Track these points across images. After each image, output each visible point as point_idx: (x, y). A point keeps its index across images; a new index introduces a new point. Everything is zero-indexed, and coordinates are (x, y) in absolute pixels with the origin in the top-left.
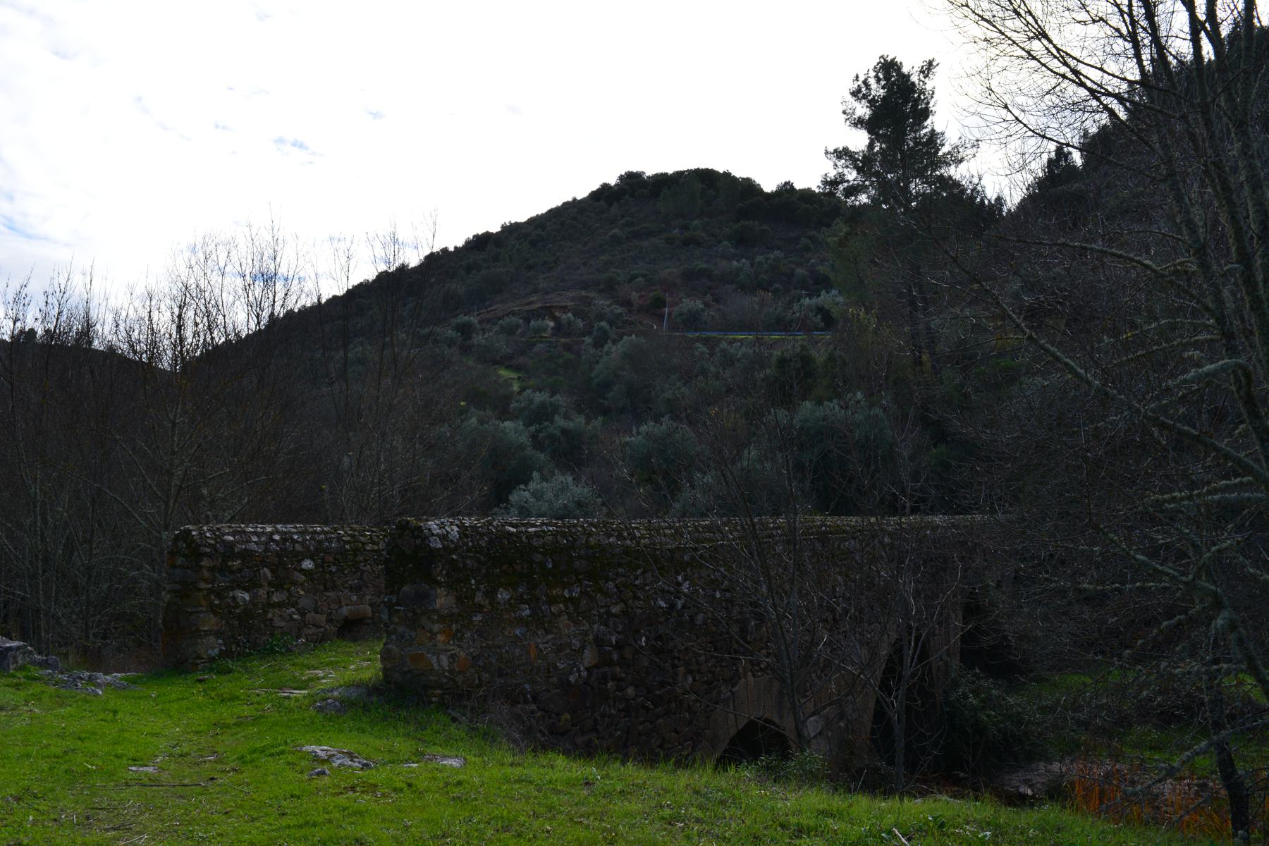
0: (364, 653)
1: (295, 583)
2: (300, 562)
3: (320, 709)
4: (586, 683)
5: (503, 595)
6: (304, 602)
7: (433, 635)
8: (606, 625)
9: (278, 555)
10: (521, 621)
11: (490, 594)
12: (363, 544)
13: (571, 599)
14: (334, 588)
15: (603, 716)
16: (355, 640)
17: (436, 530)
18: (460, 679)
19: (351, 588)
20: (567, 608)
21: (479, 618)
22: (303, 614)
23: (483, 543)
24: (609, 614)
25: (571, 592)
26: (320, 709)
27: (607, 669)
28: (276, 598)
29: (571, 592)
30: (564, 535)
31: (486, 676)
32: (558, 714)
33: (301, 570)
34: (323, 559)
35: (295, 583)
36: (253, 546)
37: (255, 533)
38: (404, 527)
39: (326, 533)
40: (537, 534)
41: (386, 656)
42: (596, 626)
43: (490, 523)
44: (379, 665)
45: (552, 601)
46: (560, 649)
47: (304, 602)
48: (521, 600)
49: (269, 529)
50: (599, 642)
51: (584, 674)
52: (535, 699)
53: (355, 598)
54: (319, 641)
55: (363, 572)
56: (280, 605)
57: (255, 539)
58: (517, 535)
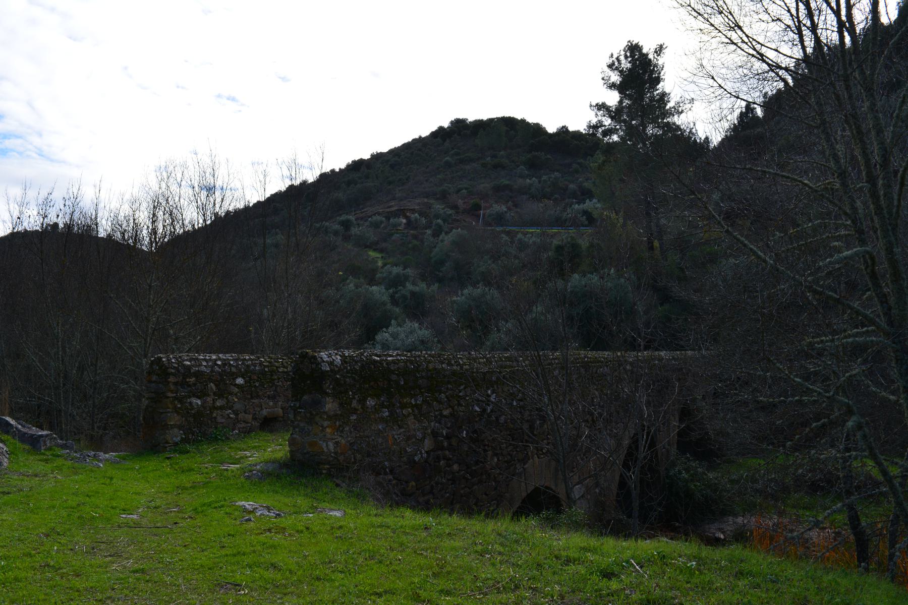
1: (231, 394)
2: (234, 379)
3: (248, 478)
5: (370, 402)
6: (237, 406)
7: (324, 429)
11: (362, 401)
12: (277, 367)
13: (416, 406)
14: (258, 397)
16: (271, 431)
17: (326, 358)
18: (341, 458)
19: (269, 397)
21: (354, 417)
22: (237, 415)
23: (357, 367)
26: (248, 478)
29: (416, 400)
30: (412, 362)
31: (359, 456)
33: (236, 385)
34: (250, 377)
35: (231, 394)
37: (205, 360)
39: (252, 360)
41: (292, 442)
42: (432, 424)
43: (362, 354)
44: (287, 448)
45: (404, 406)
46: (408, 438)
47: (237, 406)
48: (382, 406)
49: (214, 357)
50: (435, 434)
51: (425, 455)
52: (391, 471)
53: (271, 404)
54: (247, 432)
55: (277, 386)
56: (221, 408)
57: (204, 363)
58: (380, 362)
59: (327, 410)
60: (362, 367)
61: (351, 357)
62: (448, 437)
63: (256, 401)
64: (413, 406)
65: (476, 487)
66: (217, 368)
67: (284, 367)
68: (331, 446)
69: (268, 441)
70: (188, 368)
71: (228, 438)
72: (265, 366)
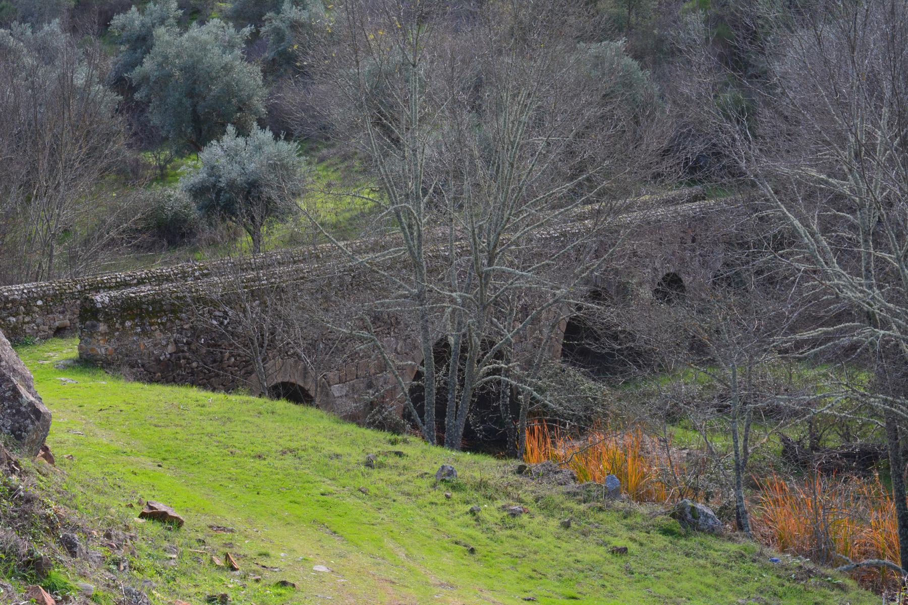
0: (499, 453)
1: (34, 312)
2: (36, 302)
3: (57, 368)
4: (169, 360)
5: (128, 324)
6: (38, 321)
7: (99, 341)
8: (181, 334)
9: (27, 300)
10: (136, 334)
11: (123, 323)
12: (65, 290)
13: (162, 323)
14: (52, 313)
15: (178, 375)
16: (62, 338)
17: (99, 300)
18: (109, 358)
19: (60, 312)
20: (159, 327)
21: (117, 334)
22: (38, 326)
23: (119, 303)
24: (182, 329)
25: (161, 320)
26: (57, 368)
27: (181, 354)
28: (27, 320)
29: (161, 320)
30: (158, 295)
31: (120, 356)
32: (154, 373)
33: (37, 306)
34: (46, 299)
35: (34, 312)
36: (16, 297)
37: (16, 290)
38: (86, 298)
39: (47, 286)
40: (145, 296)
41: (80, 348)
42: (175, 335)
43: (122, 293)
44: (77, 351)
45: (151, 324)
46: (156, 345)
47: (38, 321)
48: (137, 325)
49: (22, 287)
50: (176, 342)
51: (168, 356)
52: (143, 366)
53: (61, 317)
54: (46, 338)
55: (65, 304)
56: (28, 323)
57: (16, 293)
58: (135, 298)
59: (159, 122)
60: (123, 302)
61: (115, 297)
62: (188, 343)
63: (51, 316)
64: (159, 324)
65: (213, 379)
66: (24, 296)
67: (70, 289)
68: (103, 350)
69: (61, 345)
70: (7, 297)
71: (34, 343)
72: (56, 290)
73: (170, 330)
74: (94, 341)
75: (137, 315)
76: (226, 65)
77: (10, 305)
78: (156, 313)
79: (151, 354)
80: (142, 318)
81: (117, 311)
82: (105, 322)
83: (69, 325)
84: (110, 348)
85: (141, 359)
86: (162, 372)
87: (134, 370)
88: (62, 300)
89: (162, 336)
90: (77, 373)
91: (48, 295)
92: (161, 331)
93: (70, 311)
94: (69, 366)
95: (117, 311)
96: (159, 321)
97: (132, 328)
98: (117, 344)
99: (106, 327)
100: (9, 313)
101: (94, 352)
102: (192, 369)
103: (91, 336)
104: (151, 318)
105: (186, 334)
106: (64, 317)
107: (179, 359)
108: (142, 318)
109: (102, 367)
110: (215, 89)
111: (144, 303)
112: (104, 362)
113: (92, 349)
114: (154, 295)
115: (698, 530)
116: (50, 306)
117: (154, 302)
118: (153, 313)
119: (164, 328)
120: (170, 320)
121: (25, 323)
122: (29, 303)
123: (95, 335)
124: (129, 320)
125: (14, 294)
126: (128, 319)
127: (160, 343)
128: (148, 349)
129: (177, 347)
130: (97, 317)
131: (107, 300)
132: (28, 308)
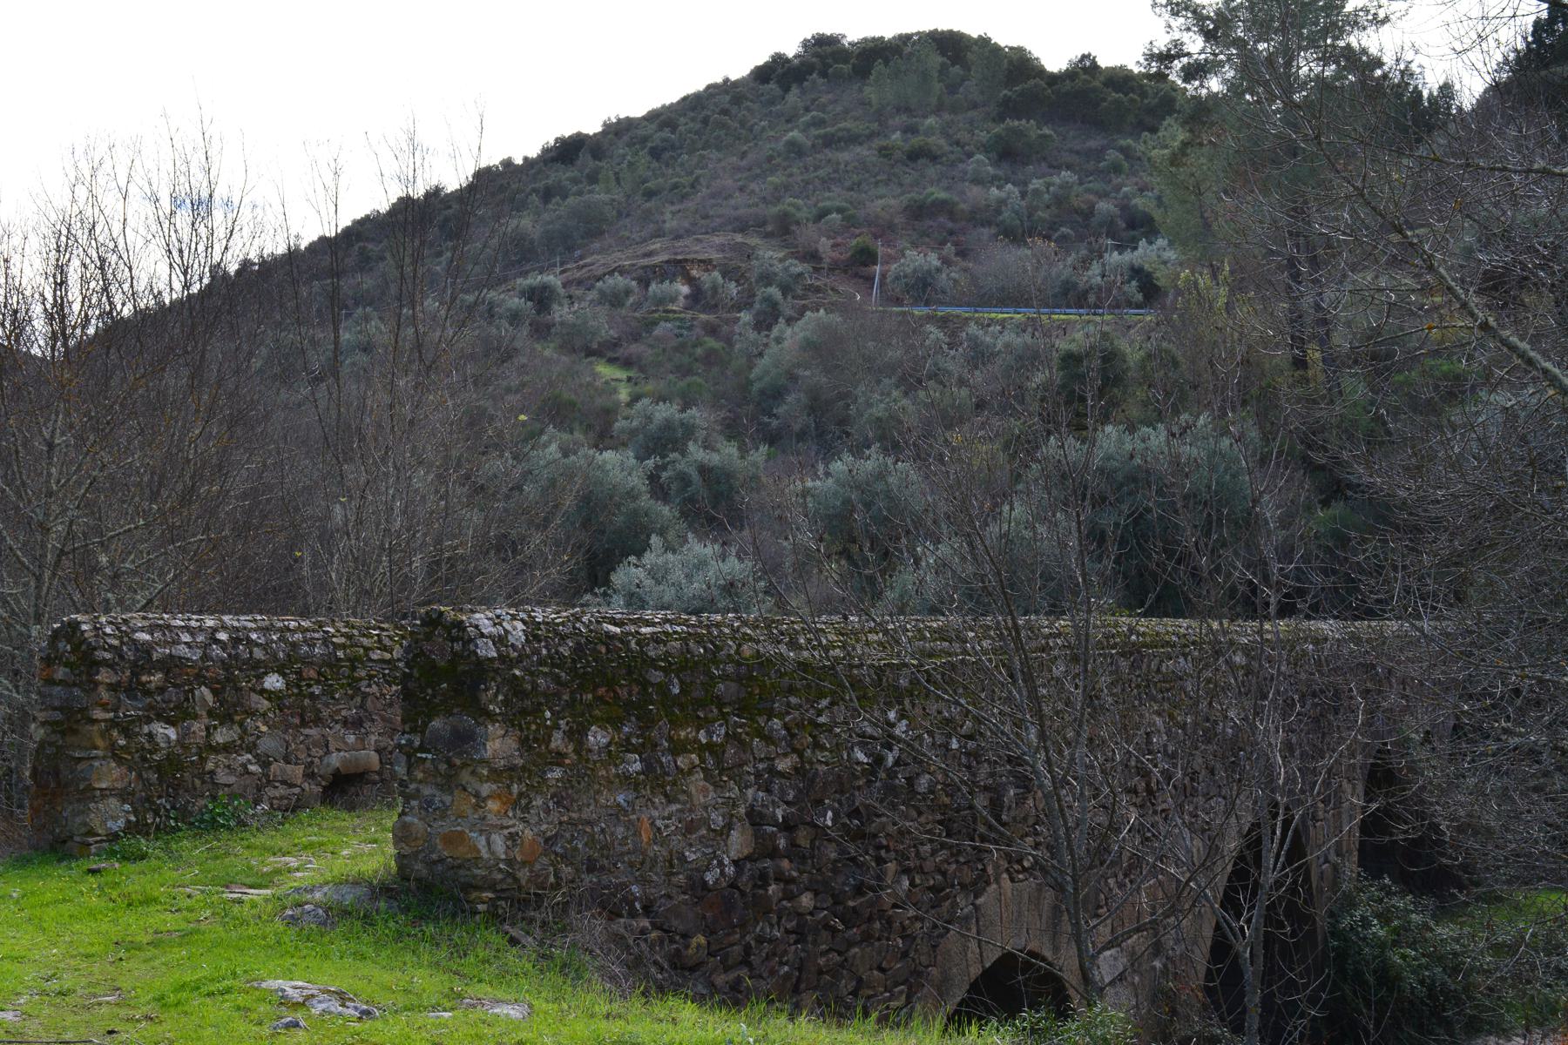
1: (252, 713)
2: (260, 677)
5: (597, 737)
7: (481, 800)
8: (768, 791)
10: (627, 780)
11: (577, 735)
12: (367, 649)
13: (710, 747)
14: (318, 721)
15: (760, 940)
16: (351, 808)
17: (488, 628)
18: (523, 875)
19: (345, 723)
20: (703, 760)
21: (556, 774)
22: (265, 764)
24: (772, 771)
27: (768, 863)
28: (221, 737)
29: (709, 734)
30: (700, 641)
31: (567, 870)
32: (685, 936)
33: (263, 692)
34: (299, 673)
35: (252, 713)
36: (182, 650)
37: (187, 629)
40: (655, 639)
41: (402, 834)
42: (750, 792)
44: (391, 850)
45: (678, 748)
46: (690, 828)
47: (267, 744)
48: (628, 747)
49: (210, 622)
50: (756, 818)
51: (730, 870)
52: (647, 910)
53: (351, 739)
54: (292, 808)
55: (365, 696)
56: (227, 748)
57: (186, 638)
58: (622, 639)
60: (578, 649)
63: (313, 732)
64: (702, 749)
66: (216, 651)
70: (145, 650)
73: (735, 773)
74: (465, 804)
75: (628, 705)
76: (632, 489)
77: (157, 678)
78: (693, 708)
79: (675, 861)
80: (647, 722)
81: (557, 679)
82: (510, 721)
83: (377, 766)
84: (528, 834)
85: (644, 881)
86: (710, 932)
87: (619, 925)
88: (354, 682)
89: (712, 794)
90: (378, 944)
91: (307, 661)
92: (708, 776)
93: (380, 725)
94: (346, 913)
95: (557, 679)
96: (702, 737)
97: (611, 755)
98: (554, 817)
99: (511, 743)
100: (150, 707)
101: (462, 851)
102: (800, 915)
103: (449, 782)
104: (675, 724)
105: (783, 792)
106: (362, 740)
107: (763, 879)
108: (647, 722)
109: (495, 918)
110: (619, 520)
111: (653, 663)
112: (501, 893)
113: (453, 839)
114: (684, 639)
115: (946, 1025)
116: (312, 696)
117: (684, 665)
118: (682, 707)
119: (720, 770)
120: (736, 736)
121: (215, 749)
122: (230, 679)
123: (465, 777)
124: (604, 722)
125: (176, 642)
126: (596, 720)
127: (705, 822)
128: (664, 842)
129: (758, 836)
130: (476, 700)
131: (518, 632)
132: (229, 695)
